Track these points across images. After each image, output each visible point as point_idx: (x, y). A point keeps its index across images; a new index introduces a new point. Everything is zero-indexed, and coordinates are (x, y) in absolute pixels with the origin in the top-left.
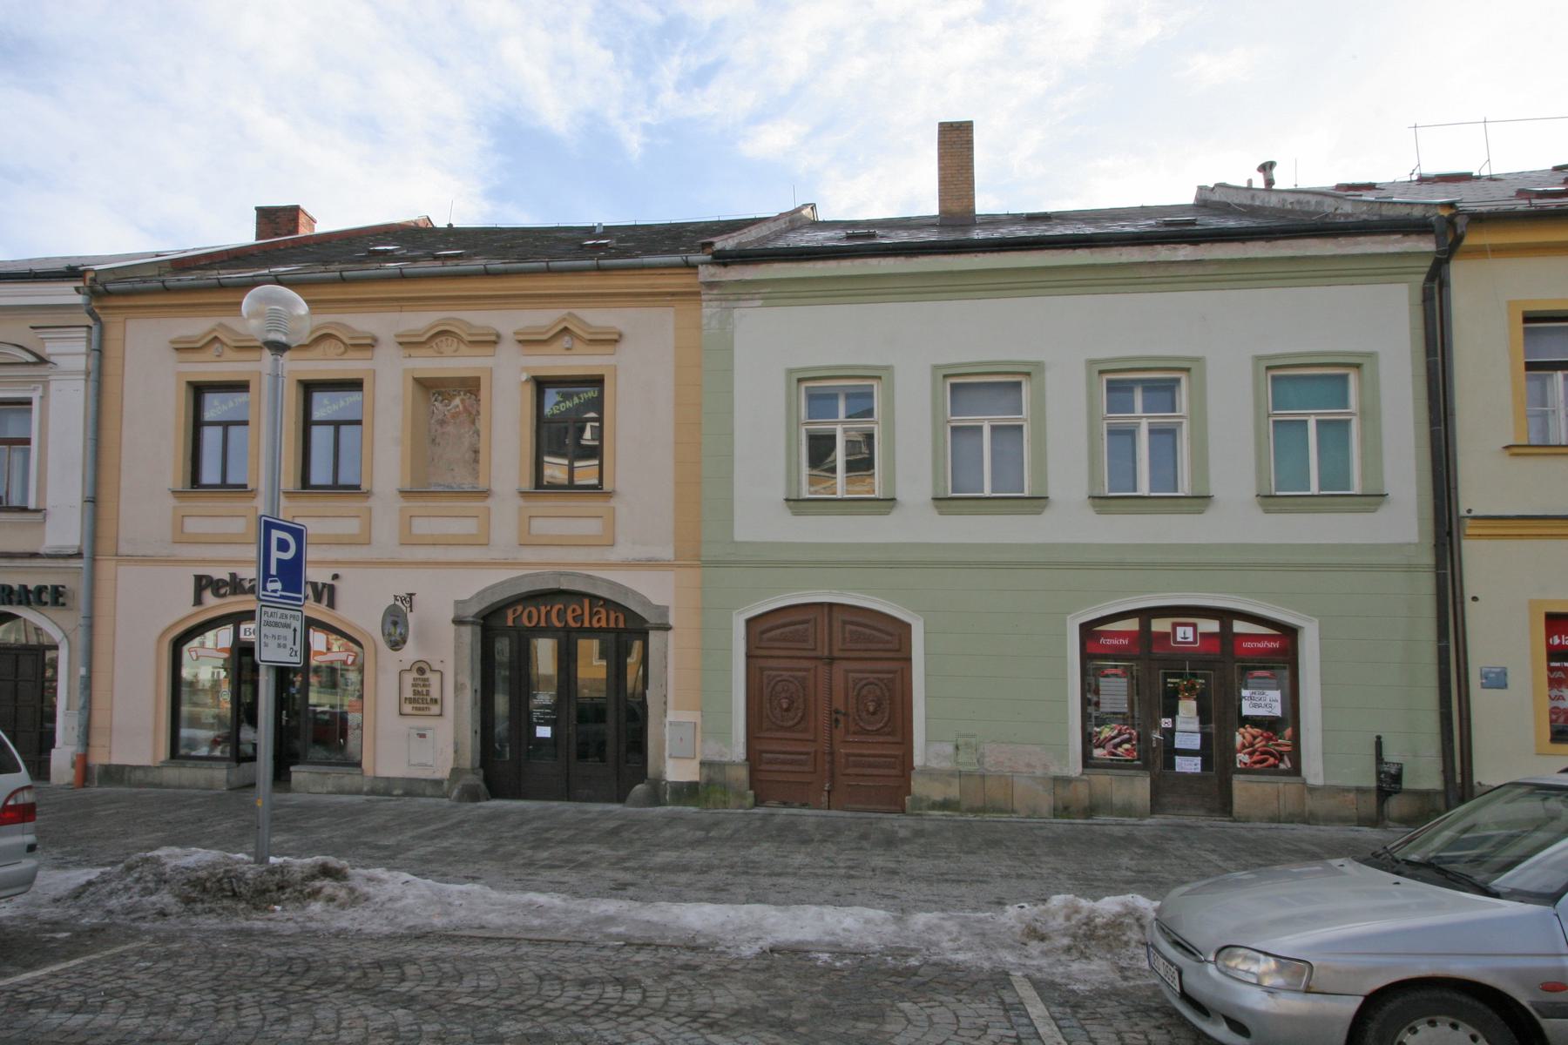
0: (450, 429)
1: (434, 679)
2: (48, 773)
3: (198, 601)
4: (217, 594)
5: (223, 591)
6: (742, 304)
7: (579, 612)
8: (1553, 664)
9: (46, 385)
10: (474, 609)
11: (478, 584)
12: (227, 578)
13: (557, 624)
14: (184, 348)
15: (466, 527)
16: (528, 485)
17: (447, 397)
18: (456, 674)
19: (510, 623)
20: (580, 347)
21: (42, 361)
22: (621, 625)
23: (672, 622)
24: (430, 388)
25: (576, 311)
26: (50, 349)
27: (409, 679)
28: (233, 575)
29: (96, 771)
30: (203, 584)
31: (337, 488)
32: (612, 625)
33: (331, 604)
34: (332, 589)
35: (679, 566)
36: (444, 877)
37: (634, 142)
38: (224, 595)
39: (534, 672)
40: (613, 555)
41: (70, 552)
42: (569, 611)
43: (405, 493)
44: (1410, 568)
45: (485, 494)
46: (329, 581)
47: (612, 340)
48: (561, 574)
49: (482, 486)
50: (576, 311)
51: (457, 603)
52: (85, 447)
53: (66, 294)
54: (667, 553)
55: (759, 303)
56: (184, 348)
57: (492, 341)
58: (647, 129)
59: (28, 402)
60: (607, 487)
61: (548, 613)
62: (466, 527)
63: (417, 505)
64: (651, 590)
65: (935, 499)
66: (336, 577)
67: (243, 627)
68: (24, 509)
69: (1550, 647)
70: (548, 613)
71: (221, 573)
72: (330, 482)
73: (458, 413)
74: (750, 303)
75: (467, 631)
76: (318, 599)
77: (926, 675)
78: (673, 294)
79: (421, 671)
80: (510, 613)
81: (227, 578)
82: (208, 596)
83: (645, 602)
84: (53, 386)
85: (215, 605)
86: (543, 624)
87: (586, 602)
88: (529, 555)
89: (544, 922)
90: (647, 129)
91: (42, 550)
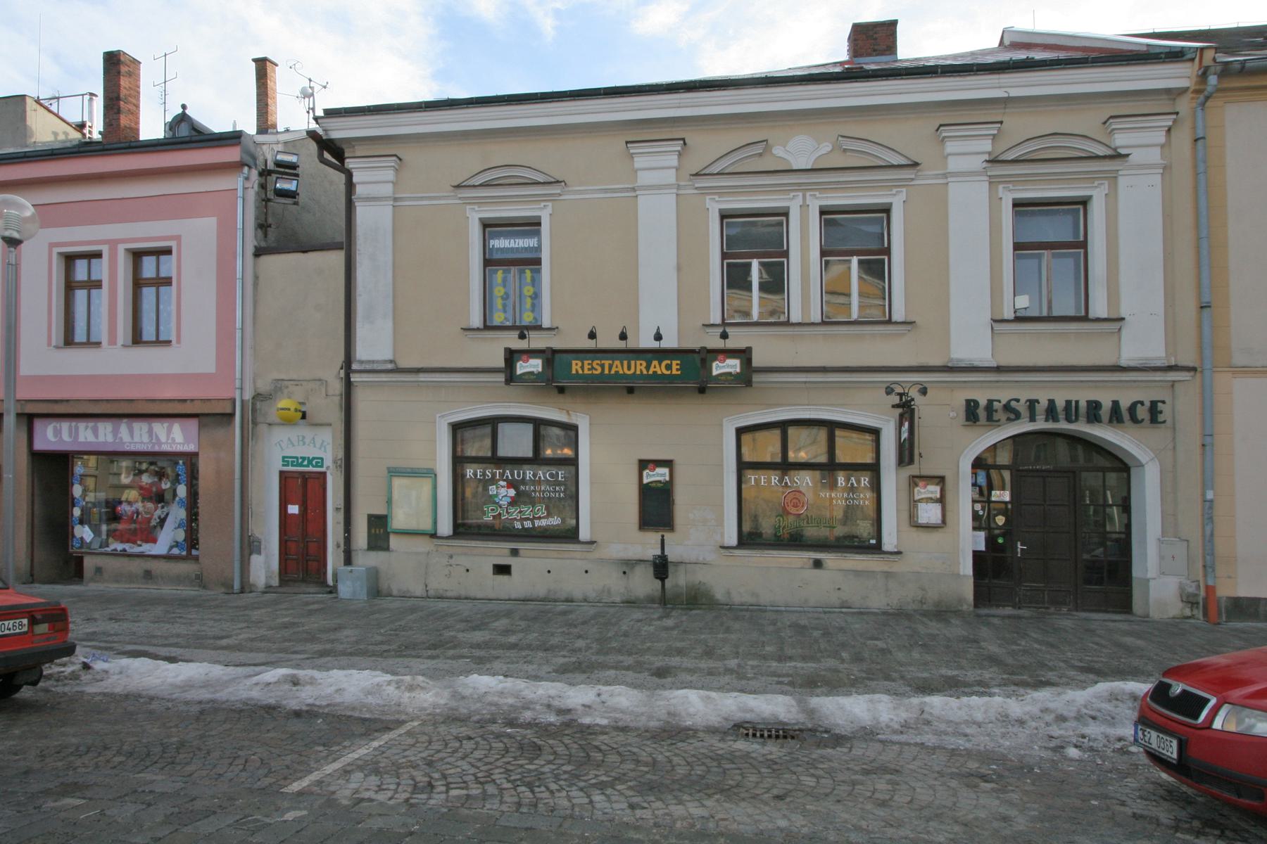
2: (1131, 608)
9: (1113, 179)
17: (74, 270)
21: (1117, 156)
26: (1121, 140)
29: (1223, 605)
31: (159, 342)
36: (213, 701)
37: (548, 25)
41: (1159, 364)
44: (754, 440)
53: (1177, 76)
58: (557, 13)
59: (1084, 202)
68: (787, 323)
72: (154, 339)
77: (592, 523)
84: (1122, 182)
89: (968, 745)
90: (557, 13)
91: (1123, 363)
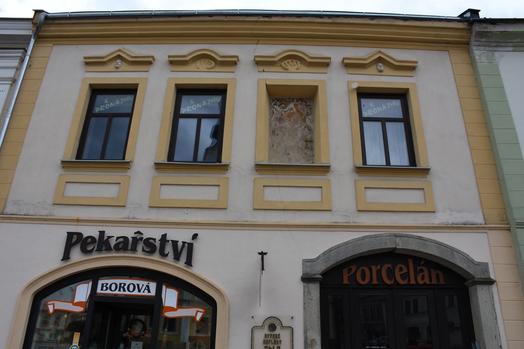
0: (287, 124)
1: (285, 336)
3: (66, 256)
4: (84, 251)
5: (90, 248)
6: (499, 49)
7: (405, 270)
8: (130, 248)
10: (320, 268)
11: (320, 246)
12: (96, 235)
13: (388, 282)
14: (91, 63)
15: (311, 196)
16: (163, 159)
18: (305, 332)
19: (346, 281)
20: (387, 71)
22: (442, 282)
23: (492, 277)
24: (277, 96)
25: (383, 50)
27: (260, 336)
28: (102, 233)
30: (73, 240)
32: (434, 282)
33: (189, 263)
34: (191, 246)
35: (490, 229)
38: (91, 251)
39: (46, 299)
40: (439, 219)
42: (397, 270)
43: (260, 168)
45: (326, 169)
46: (189, 240)
47: (410, 68)
48: (396, 236)
49: (323, 162)
50: (383, 50)
51: (305, 261)
52: (416, 136)
54: (478, 219)
55: (511, 49)
56: (91, 63)
57: (323, 64)
60: (422, 164)
61: (379, 272)
62: (311, 196)
63: (269, 178)
64: (475, 249)
65: (63, 162)
66: (195, 236)
67: (100, 282)
69: (186, 242)
70: (379, 272)
71: (90, 231)
73: (293, 114)
74: (505, 49)
75: (315, 289)
76: (177, 257)
78: (448, 43)
79: (272, 327)
80: (345, 271)
81: (96, 235)
82: (76, 254)
83: (470, 260)
85: (80, 261)
86: (375, 282)
87: (411, 262)
88: (366, 219)
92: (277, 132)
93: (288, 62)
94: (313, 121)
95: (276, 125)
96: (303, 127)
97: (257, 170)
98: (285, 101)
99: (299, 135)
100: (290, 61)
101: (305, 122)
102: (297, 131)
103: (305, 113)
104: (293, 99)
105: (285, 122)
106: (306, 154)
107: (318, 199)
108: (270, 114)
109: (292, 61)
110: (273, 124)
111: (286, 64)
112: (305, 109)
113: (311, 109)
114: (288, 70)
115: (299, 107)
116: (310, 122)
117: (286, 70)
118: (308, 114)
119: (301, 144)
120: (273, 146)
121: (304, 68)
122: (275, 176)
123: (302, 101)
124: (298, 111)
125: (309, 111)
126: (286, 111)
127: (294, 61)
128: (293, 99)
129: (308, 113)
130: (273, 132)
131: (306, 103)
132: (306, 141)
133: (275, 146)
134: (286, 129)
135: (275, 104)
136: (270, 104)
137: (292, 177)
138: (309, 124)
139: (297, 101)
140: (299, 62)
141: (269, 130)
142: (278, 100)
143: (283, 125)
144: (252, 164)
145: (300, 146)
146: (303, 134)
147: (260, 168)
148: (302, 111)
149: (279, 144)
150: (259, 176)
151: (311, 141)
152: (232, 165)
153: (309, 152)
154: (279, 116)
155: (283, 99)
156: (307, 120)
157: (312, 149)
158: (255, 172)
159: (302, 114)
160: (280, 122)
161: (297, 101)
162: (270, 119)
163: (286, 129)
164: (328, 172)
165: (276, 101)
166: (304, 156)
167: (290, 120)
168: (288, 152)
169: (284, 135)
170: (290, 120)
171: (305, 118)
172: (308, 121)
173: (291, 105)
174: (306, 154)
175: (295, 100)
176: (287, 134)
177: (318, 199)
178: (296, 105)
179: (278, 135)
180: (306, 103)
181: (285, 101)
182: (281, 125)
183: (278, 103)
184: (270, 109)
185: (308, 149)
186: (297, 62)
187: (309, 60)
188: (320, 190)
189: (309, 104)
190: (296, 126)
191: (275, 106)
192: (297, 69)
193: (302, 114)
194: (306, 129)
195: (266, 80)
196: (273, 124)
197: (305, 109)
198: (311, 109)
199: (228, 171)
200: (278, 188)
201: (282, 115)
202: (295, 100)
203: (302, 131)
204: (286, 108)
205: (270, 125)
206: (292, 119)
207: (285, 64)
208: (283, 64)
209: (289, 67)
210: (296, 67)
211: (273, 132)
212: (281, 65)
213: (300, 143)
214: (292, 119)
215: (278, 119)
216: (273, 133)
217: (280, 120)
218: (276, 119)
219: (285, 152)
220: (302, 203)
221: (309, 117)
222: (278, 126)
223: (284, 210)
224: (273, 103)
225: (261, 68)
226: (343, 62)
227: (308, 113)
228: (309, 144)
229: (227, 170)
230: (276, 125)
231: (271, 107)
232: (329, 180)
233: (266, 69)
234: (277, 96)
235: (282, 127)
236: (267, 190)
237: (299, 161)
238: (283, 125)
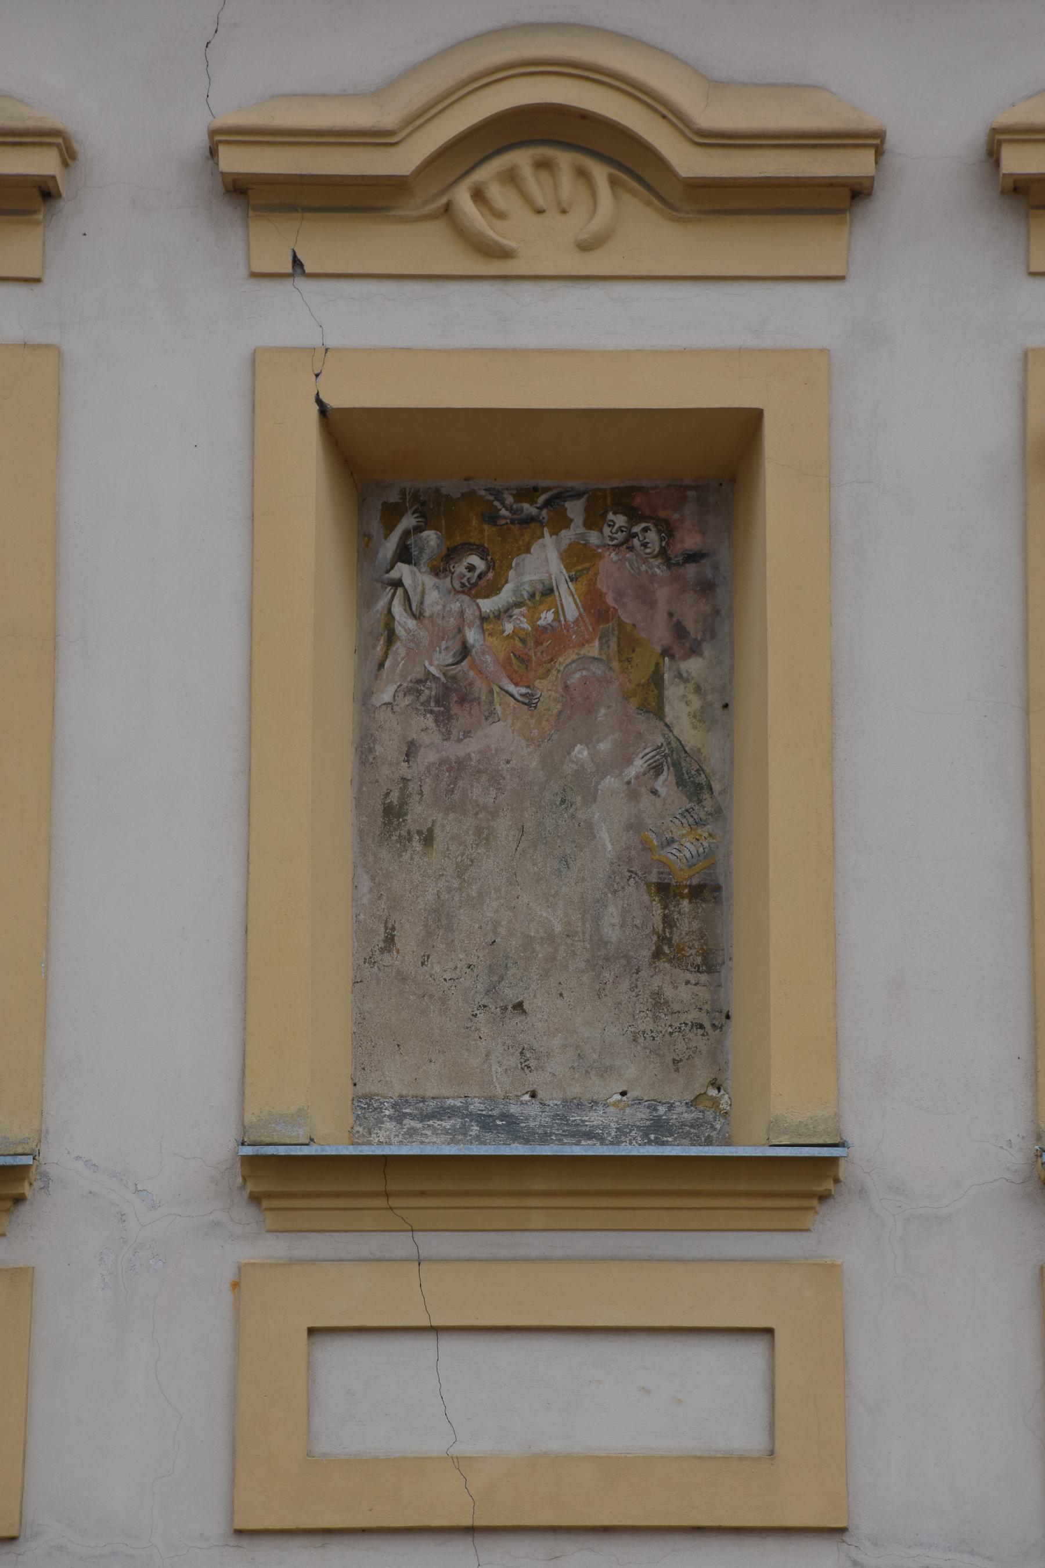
0: (501, 737)
24: (416, 491)
43: (280, 1179)
45: (804, 1179)
63: (355, 1264)
73: (551, 640)
92: (419, 813)
93: (511, 178)
94: (721, 707)
95: (411, 750)
96: (639, 765)
97: (255, 1199)
98: (492, 518)
99: (608, 841)
100: (522, 159)
101: (659, 713)
102: (591, 797)
103: (660, 634)
104: (557, 499)
105: (491, 716)
106: (658, 1002)
107: (746, 1436)
108: (362, 650)
109: (543, 165)
110: (389, 746)
111: (496, 193)
112: (663, 594)
113: (706, 588)
114: (505, 254)
115: (613, 570)
116: (701, 718)
117: (491, 259)
118: (684, 641)
119: (624, 918)
120: (390, 940)
121: (649, 237)
122: (400, 1244)
123: (634, 515)
124: (597, 609)
125: (690, 611)
126: (498, 616)
127: (565, 159)
128: (557, 499)
129: (679, 631)
130: (393, 813)
131: (667, 529)
132: (665, 891)
133: (408, 942)
134: (495, 779)
135: (404, 554)
136: (363, 546)
137: (535, 1244)
138: (688, 733)
139: (594, 520)
140: (600, 173)
141: (359, 801)
142: (431, 507)
143: (472, 747)
144: (217, 1143)
145: (612, 934)
146: (635, 826)
147: (280, 1179)
148: (629, 613)
149: (440, 918)
150: (276, 1248)
151: (707, 891)
152: (57, 1158)
153: (683, 990)
154: (438, 661)
155: (470, 497)
156: (673, 691)
157: (710, 961)
158: (245, 1213)
159: (628, 643)
160: (444, 719)
161: (594, 520)
162: (364, 698)
163: (495, 779)
164: (823, 1197)
165: (409, 521)
166: (645, 1024)
167: (530, 702)
168: (511, 994)
169: (484, 836)
170: (530, 702)
171: (657, 679)
172: (680, 705)
173: (543, 561)
174: (658, 1002)
175: (575, 509)
176: (503, 827)
177: (746, 1436)
178: (579, 559)
179: (428, 840)
180: (667, 529)
181: (492, 518)
182: (454, 750)
183: (431, 537)
184: (365, 600)
185: (678, 960)
186: (582, 173)
187: (689, 162)
188: (753, 1351)
189: (689, 541)
190: (581, 752)
191: (403, 571)
192: (585, 247)
193: (628, 643)
194: (665, 783)
195: (320, 358)
196: (389, 746)
197: (663, 594)
198: (706, 588)
199: (24, 1209)
200: (423, 1348)
201: (465, 651)
202: (575, 509)
203: (633, 796)
204: (493, 590)
205: (365, 750)
206: (546, 688)
207: (478, 195)
208: (463, 198)
209: (516, 229)
210: (575, 225)
211: (393, 813)
212: (447, 209)
213: (612, 914)
214: (546, 688)
215: (430, 690)
216: (388, 820)
217: (448, 699)
218: (415, 689)
219: (492, 990)
220: (613, 1466)
221: (693, 666)
222: (428, 757)
223: (471, 1530)
224: (390, 545)
225: (274, 241)
226: (993, 154)
227: (679, 631)
228: (688, 913)
229: (19, 1200)
230: (411, 750)
231: (371, 581)
232: (830, 1273)
233: (324, 244)
234: (416, 491)
235: (459, 767)
236: (343, 1363)
237: (606, 1071)
238: (472, 747)
